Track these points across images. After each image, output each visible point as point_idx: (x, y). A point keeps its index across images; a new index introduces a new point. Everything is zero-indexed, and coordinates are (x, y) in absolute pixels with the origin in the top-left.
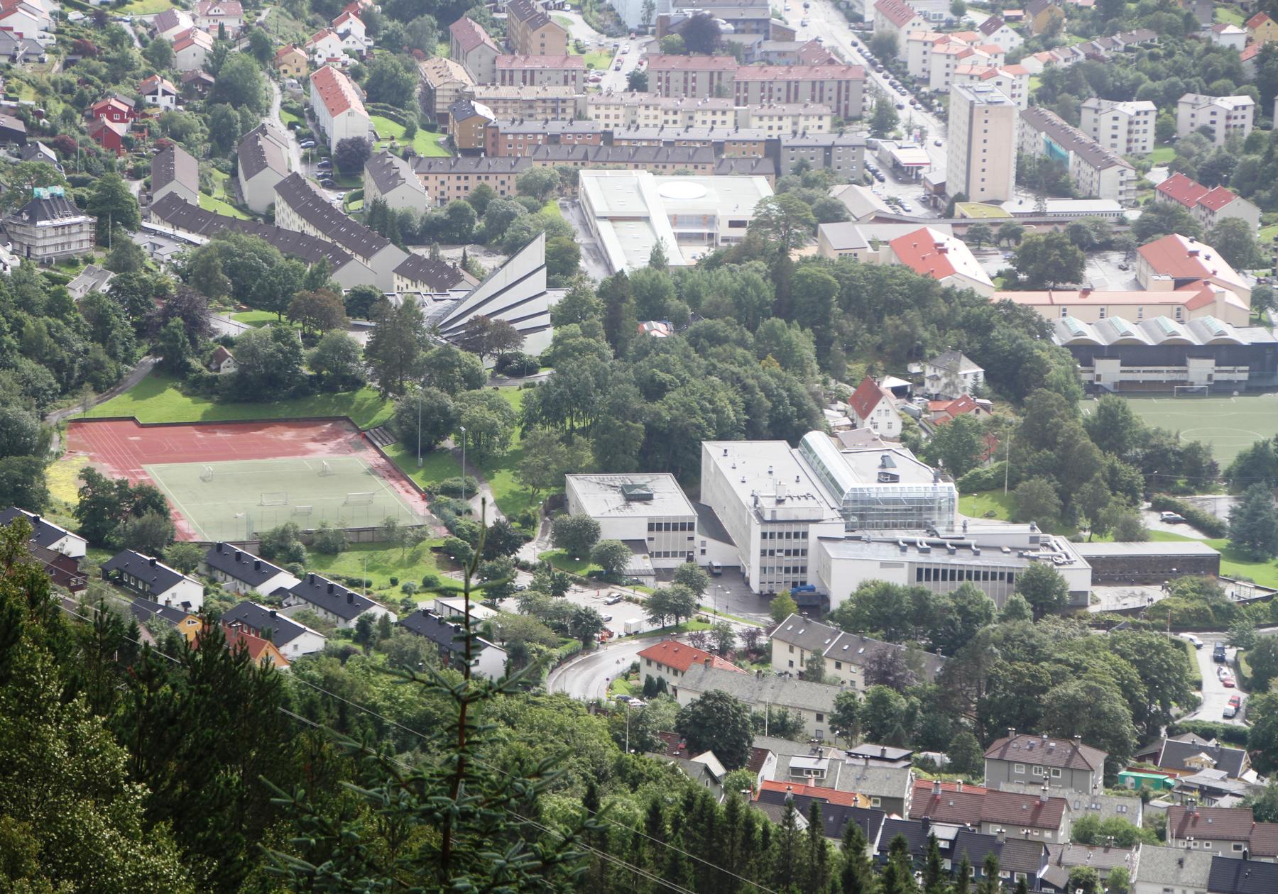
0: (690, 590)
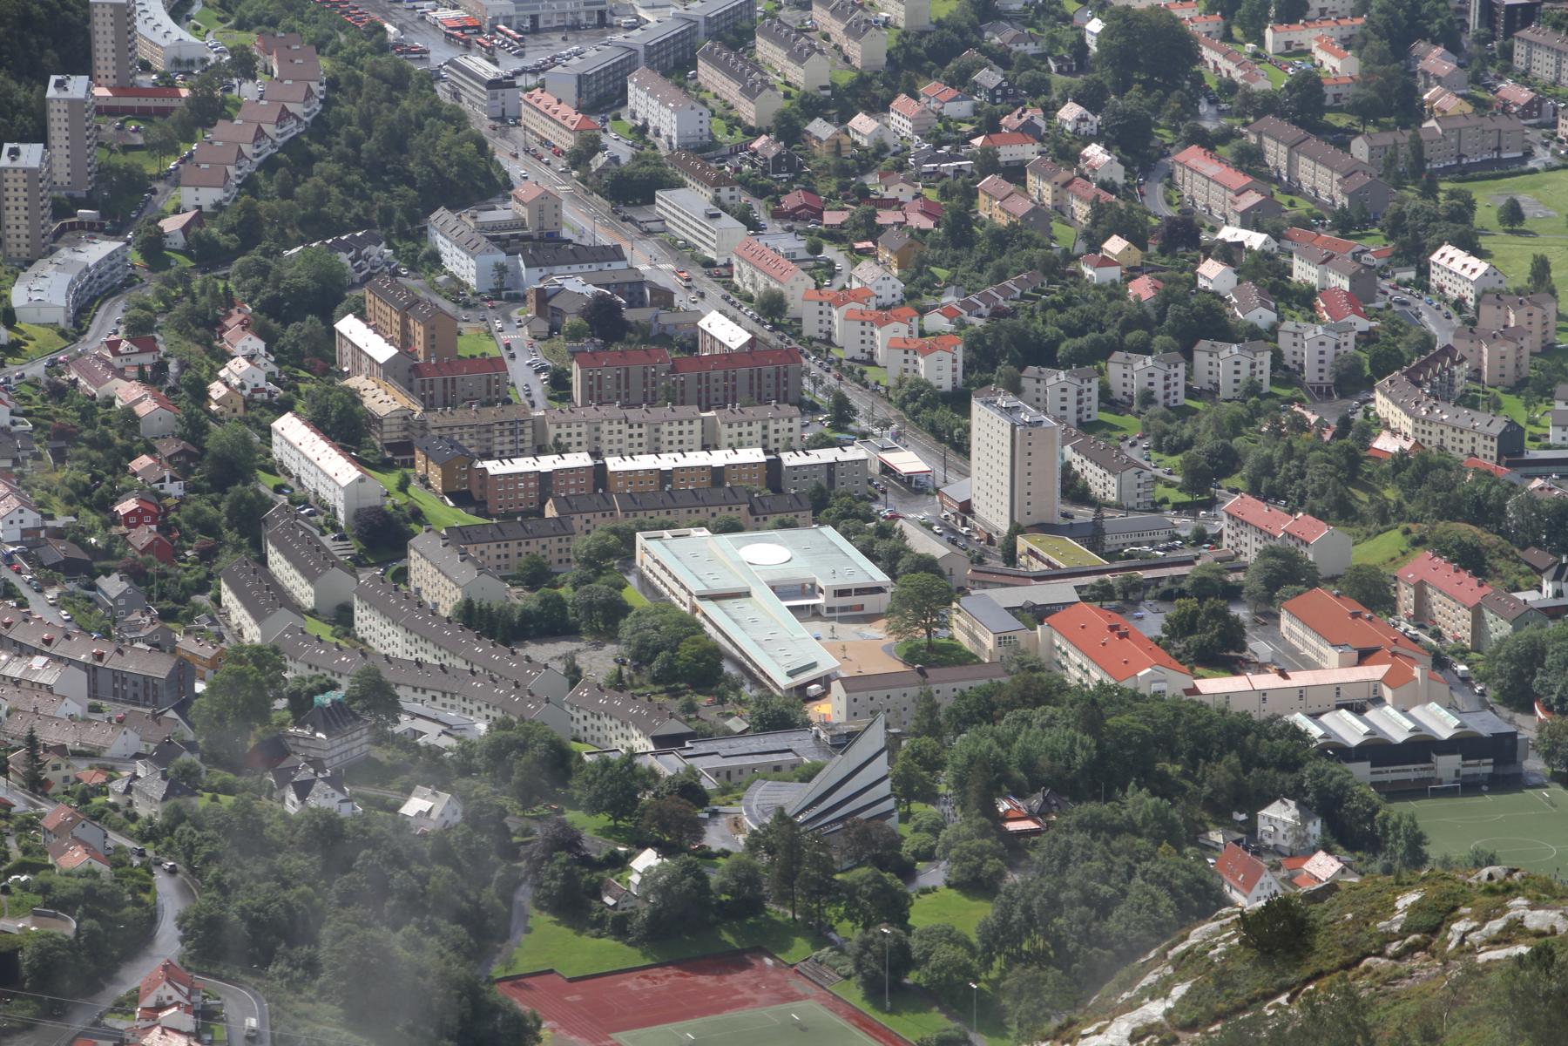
0: (1170, 1004)
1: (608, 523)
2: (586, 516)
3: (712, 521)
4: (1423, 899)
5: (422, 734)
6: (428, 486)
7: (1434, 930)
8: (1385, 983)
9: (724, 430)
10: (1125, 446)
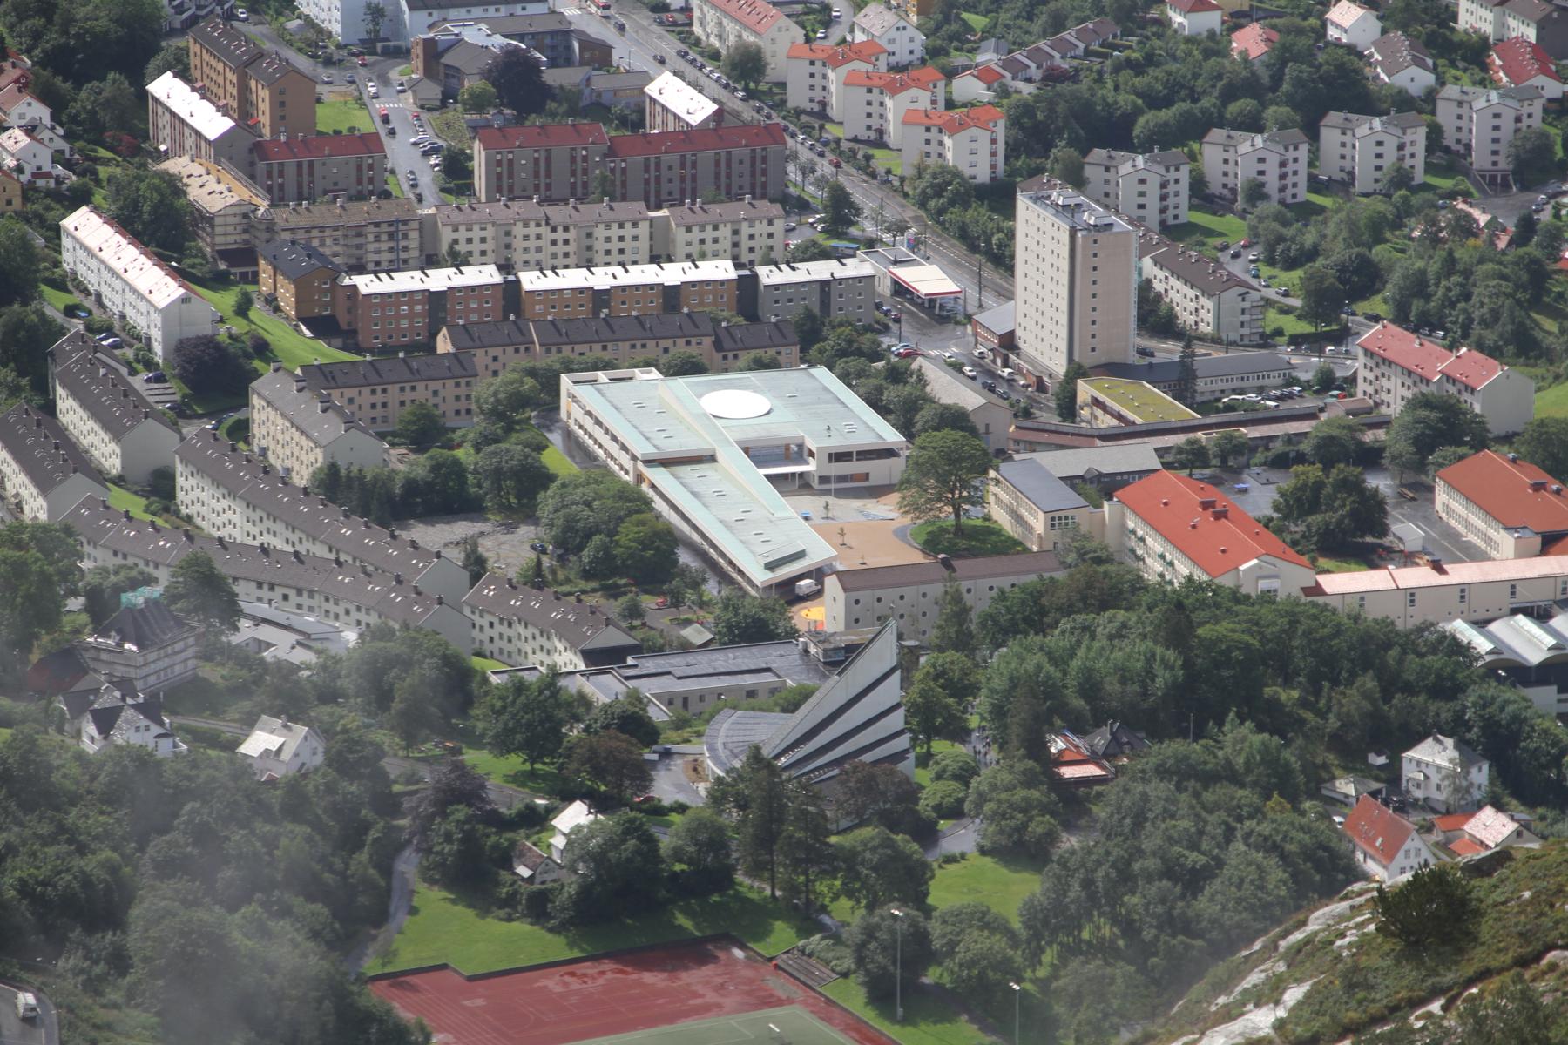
0: (1281, 1013)
1: (523, 361)
2: (493, 352)
3: (664, 359)
5: (269, 645)
6: (277, 309)
9: (680, 235)
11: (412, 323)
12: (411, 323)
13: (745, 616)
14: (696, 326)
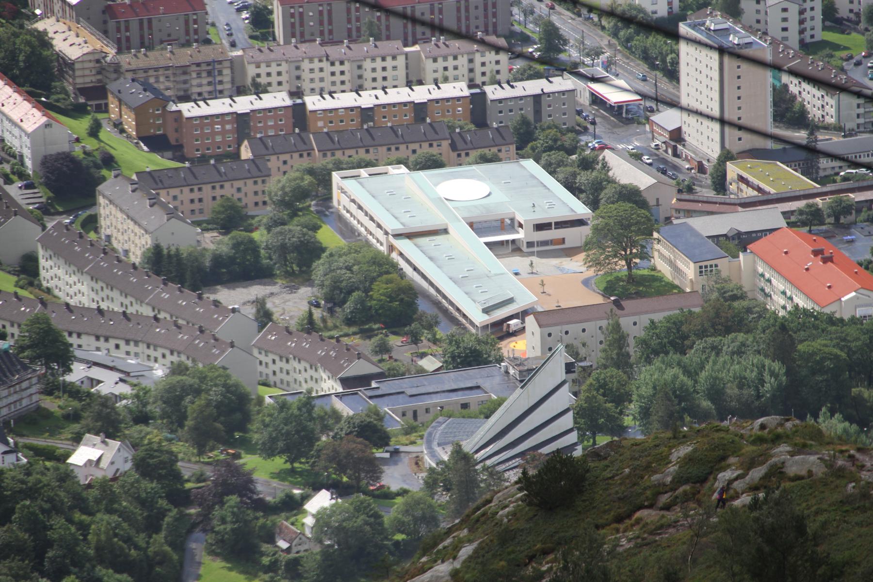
0: (457, 565)
1: (305, 163)
2: (283, 157)
3: (412, 158)
4: (695, 451)
5: (99, 382)
6: (122, 131)
7: (702, 480)
8: (652, 533)
9: (429, 65)
10: (848, 66)
11: (222, 136)
12: (224, 138)
13: (465, 348)
14: (436, 133)
